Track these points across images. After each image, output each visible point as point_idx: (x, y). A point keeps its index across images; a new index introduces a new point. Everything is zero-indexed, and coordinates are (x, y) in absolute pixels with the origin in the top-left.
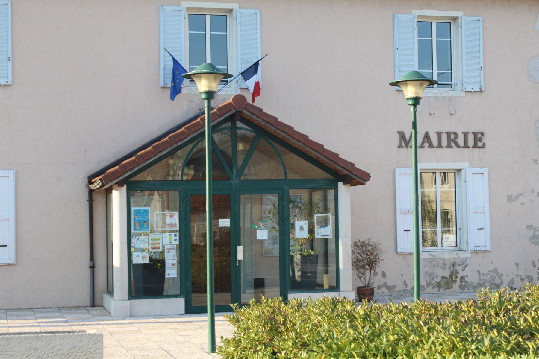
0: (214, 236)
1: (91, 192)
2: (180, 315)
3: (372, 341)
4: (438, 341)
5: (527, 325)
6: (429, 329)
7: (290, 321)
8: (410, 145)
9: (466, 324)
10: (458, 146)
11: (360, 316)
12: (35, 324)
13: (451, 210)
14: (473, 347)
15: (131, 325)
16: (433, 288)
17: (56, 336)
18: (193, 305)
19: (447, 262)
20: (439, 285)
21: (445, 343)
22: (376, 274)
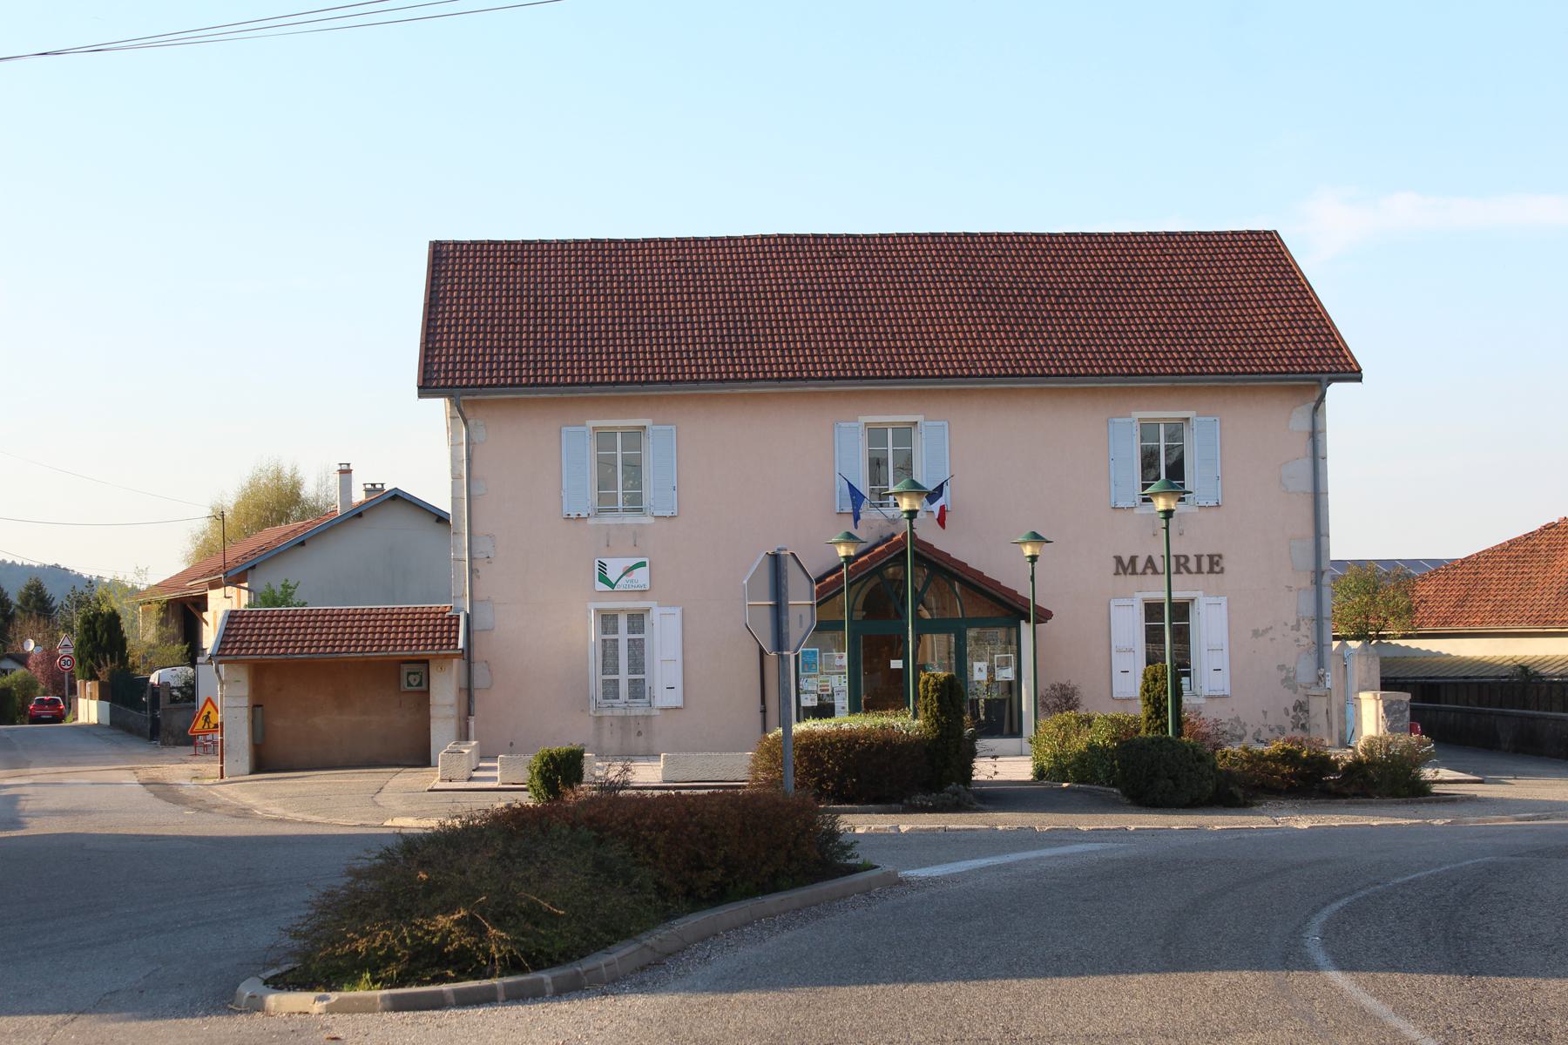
10: (1189, 571)
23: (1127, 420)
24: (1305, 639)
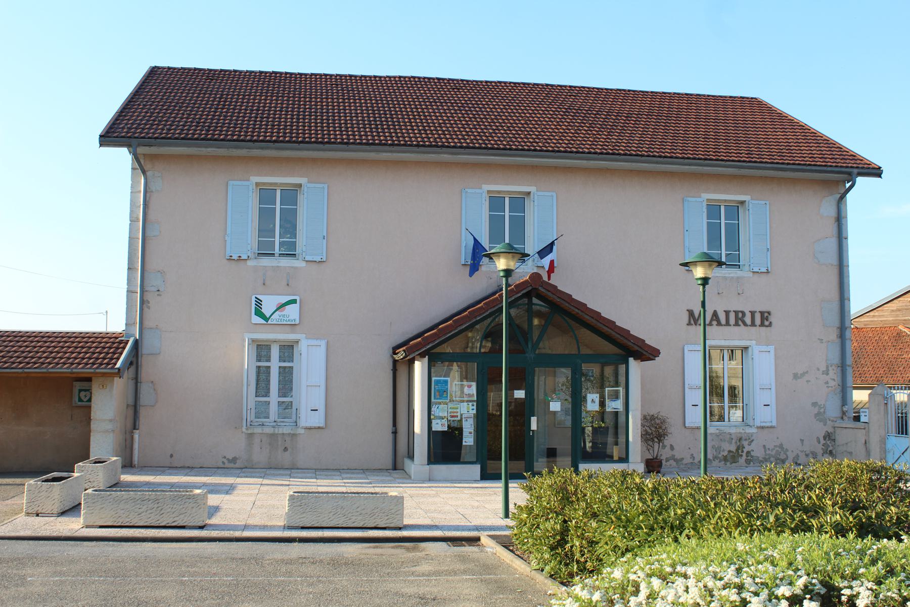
0: (510, 406)
1: (395, 362)
2: (476, 481)
3: (660, 514)
4: (724, 517)
5: (811, 503)
6: (715, 504)
7: (581, 491)
8: (699, 322)
9: (752, 500)
10: (745, 324)
11: (649, 489)
12: (341, 484)
13: (738, 386)
14: (758, 523)
15: (430, 489)
16: (720, 462)
17: (360, 496)
18: (488, 472)
19: (733, 436)
20: (725, 459)
21: (731, 519)
22: (664, 447)
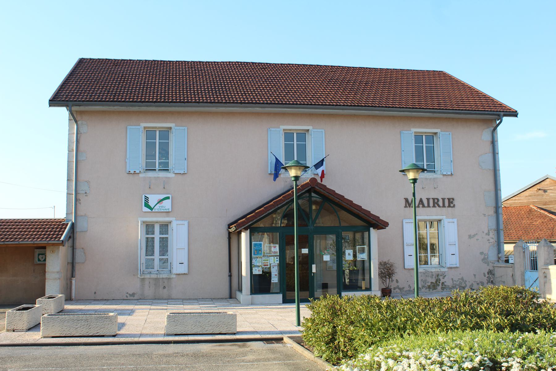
10: (439, 206)
23: (409, 132)
24: (492, 239)
